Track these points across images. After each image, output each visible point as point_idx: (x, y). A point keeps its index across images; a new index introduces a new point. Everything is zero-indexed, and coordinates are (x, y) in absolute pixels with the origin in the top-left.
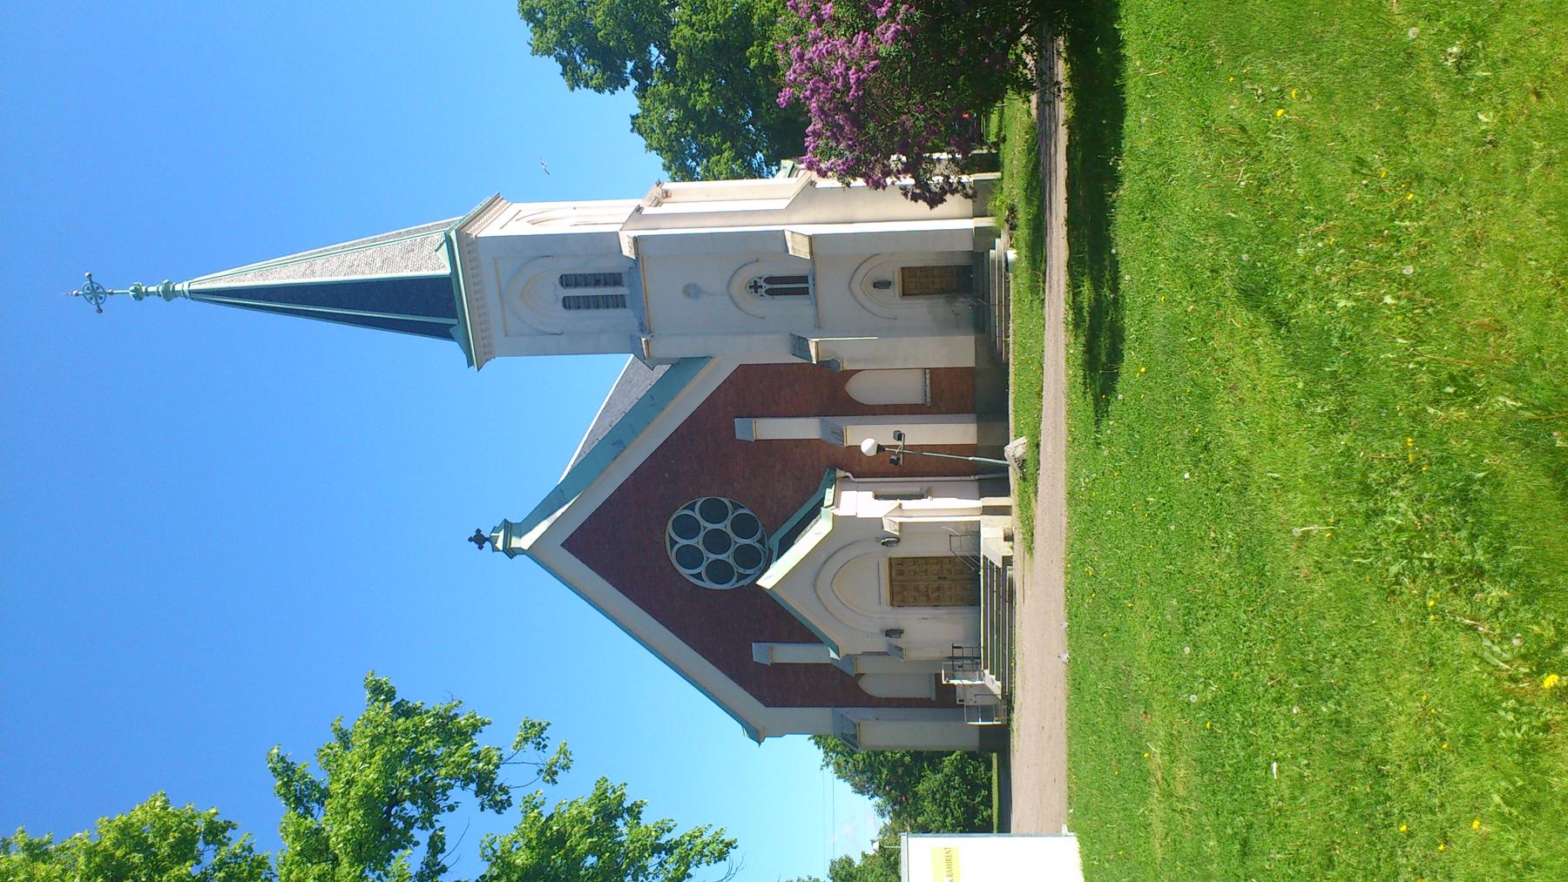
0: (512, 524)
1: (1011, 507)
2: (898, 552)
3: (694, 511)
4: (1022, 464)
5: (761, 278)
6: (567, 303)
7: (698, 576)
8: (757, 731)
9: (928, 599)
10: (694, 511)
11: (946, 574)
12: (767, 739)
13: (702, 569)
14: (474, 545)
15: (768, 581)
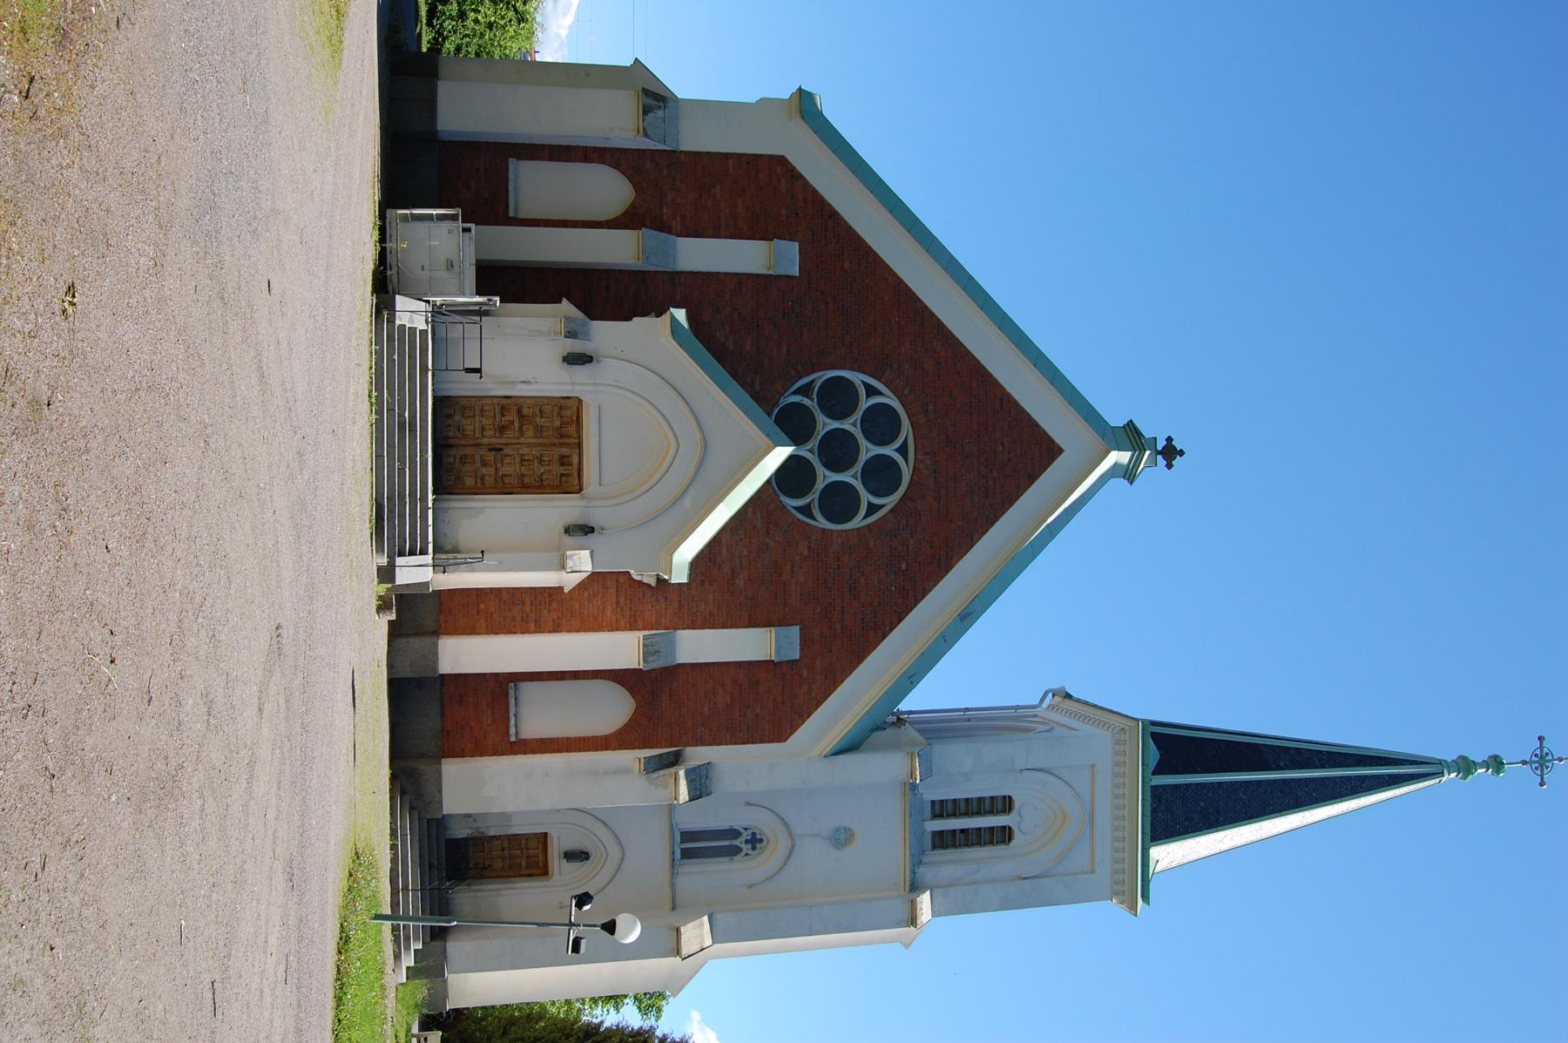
0: (1124, 477)
1: (389, 621)
3: (869, 502)
5: (747, 854)
6: (1004, 804)
7: (871, 391)
8: (803, 118)
9: (519, 411)
11: (491, 456)
12: (787, 96)
13: (865, 403)
14: (1177, 444)
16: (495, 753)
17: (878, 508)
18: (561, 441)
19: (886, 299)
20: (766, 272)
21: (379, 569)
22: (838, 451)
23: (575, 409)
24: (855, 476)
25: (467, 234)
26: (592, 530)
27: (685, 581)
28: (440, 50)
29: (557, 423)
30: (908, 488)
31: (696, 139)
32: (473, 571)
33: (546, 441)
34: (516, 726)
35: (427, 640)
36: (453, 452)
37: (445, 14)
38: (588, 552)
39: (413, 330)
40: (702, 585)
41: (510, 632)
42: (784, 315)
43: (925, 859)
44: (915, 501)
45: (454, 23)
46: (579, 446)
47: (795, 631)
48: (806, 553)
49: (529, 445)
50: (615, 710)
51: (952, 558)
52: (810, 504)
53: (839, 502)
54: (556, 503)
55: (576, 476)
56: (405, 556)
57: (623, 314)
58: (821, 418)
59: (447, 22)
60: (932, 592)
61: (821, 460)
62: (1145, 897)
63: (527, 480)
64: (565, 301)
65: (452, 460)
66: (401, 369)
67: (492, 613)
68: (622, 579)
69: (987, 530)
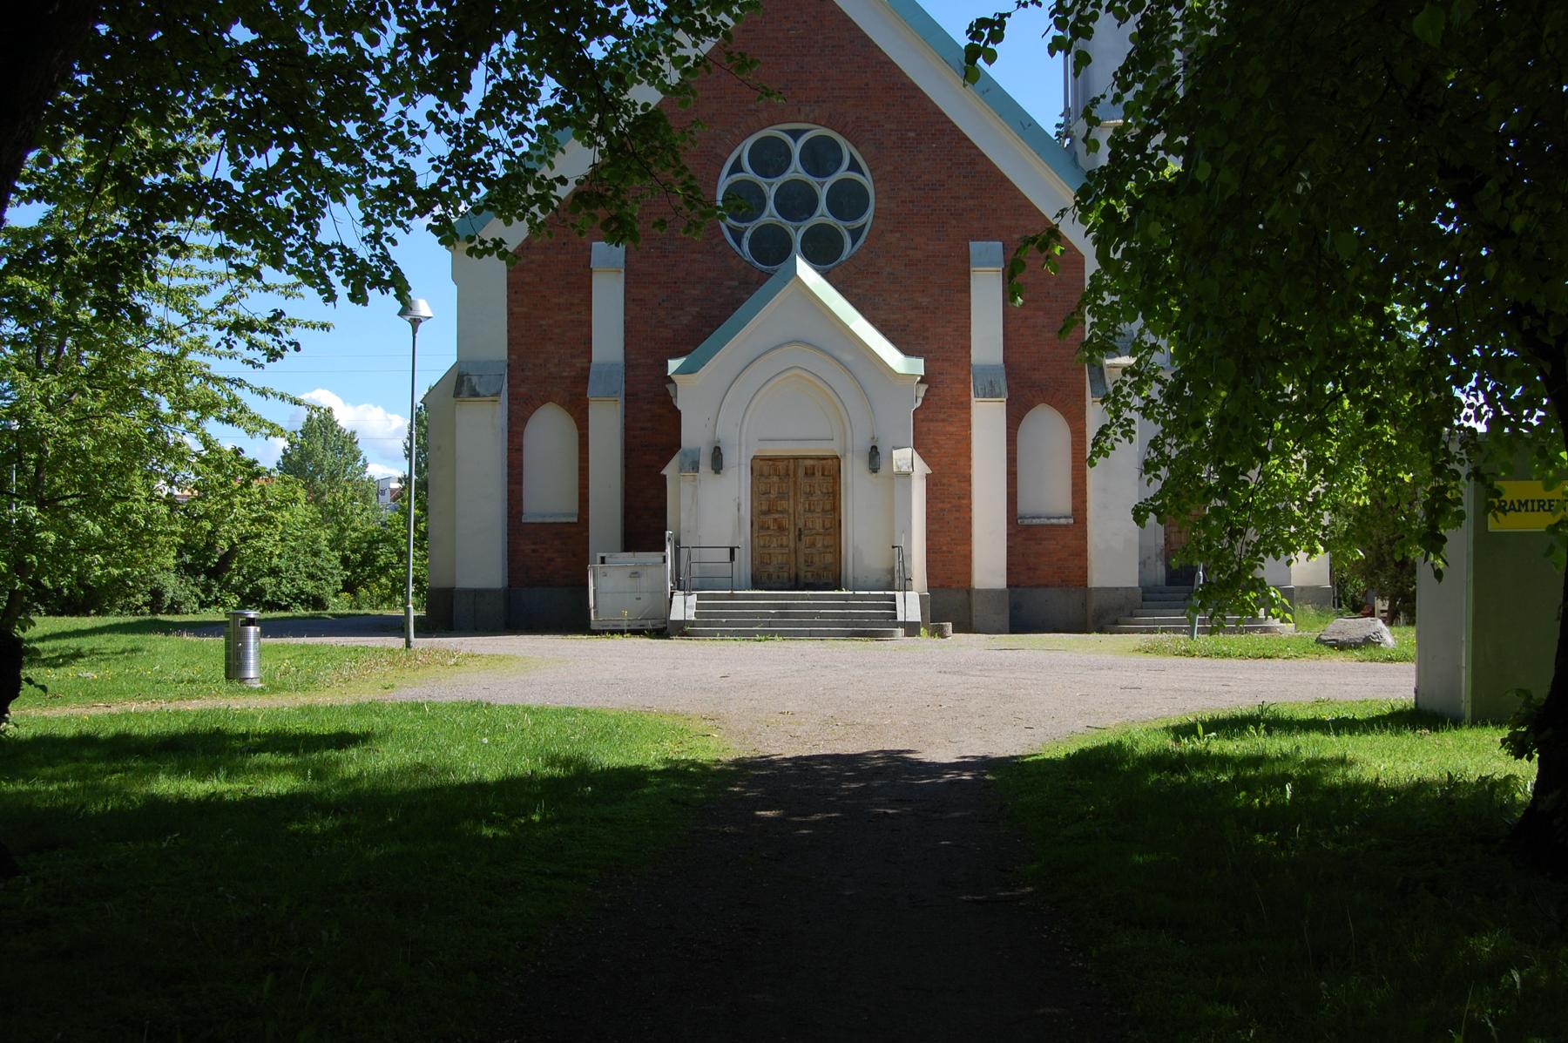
2: (854, 476)
4: (1368, 642)
7: (736, 167)
10: (848, 169)
11: (806, 540)
13: (749, 174)
15: (806, 272)
16: (1085, 538)
17: (853, 161)
18: (792, 476)
20: (623, 275)
21: (907, 635)
22: (796, 202)
23: (761, 463)
24: (822, 184)
25: (606, 560)
26: (874, 448)
27: (923, 360)
28: (314, 597)
29: (775, 479)
31: (496, 345)
32: (910, 556)
33: (792, 488)
34: (1059, 518)
35: (974, 597)
36: (802, 574)
37: (275, 593)
38: (894, 452)
39: (698, 606)
40: (927, 338)
41: (970, 523)
42: (664, 257)
44: (847, 123)
45: (284, 580)
46: (796, 458)
47: (975, 246)
48: (898, 235)
49: (796, 504)
50: (1047, 426)
51: (904, 84)
52: (849, 231)
53: (847, 200)
54: (849, 480)
55: (824, 462)
56: (895, 605)
57: (673, 417)
58: (764, 219)
59: (284, 589)
60: (938, 104)
61: (806, 219)
63: (828, 507)
64: (664, 472)
65: (809, 574)
66: (733, 616)
67: (952, 540)
68: (920, 416)
69: (876, 46)
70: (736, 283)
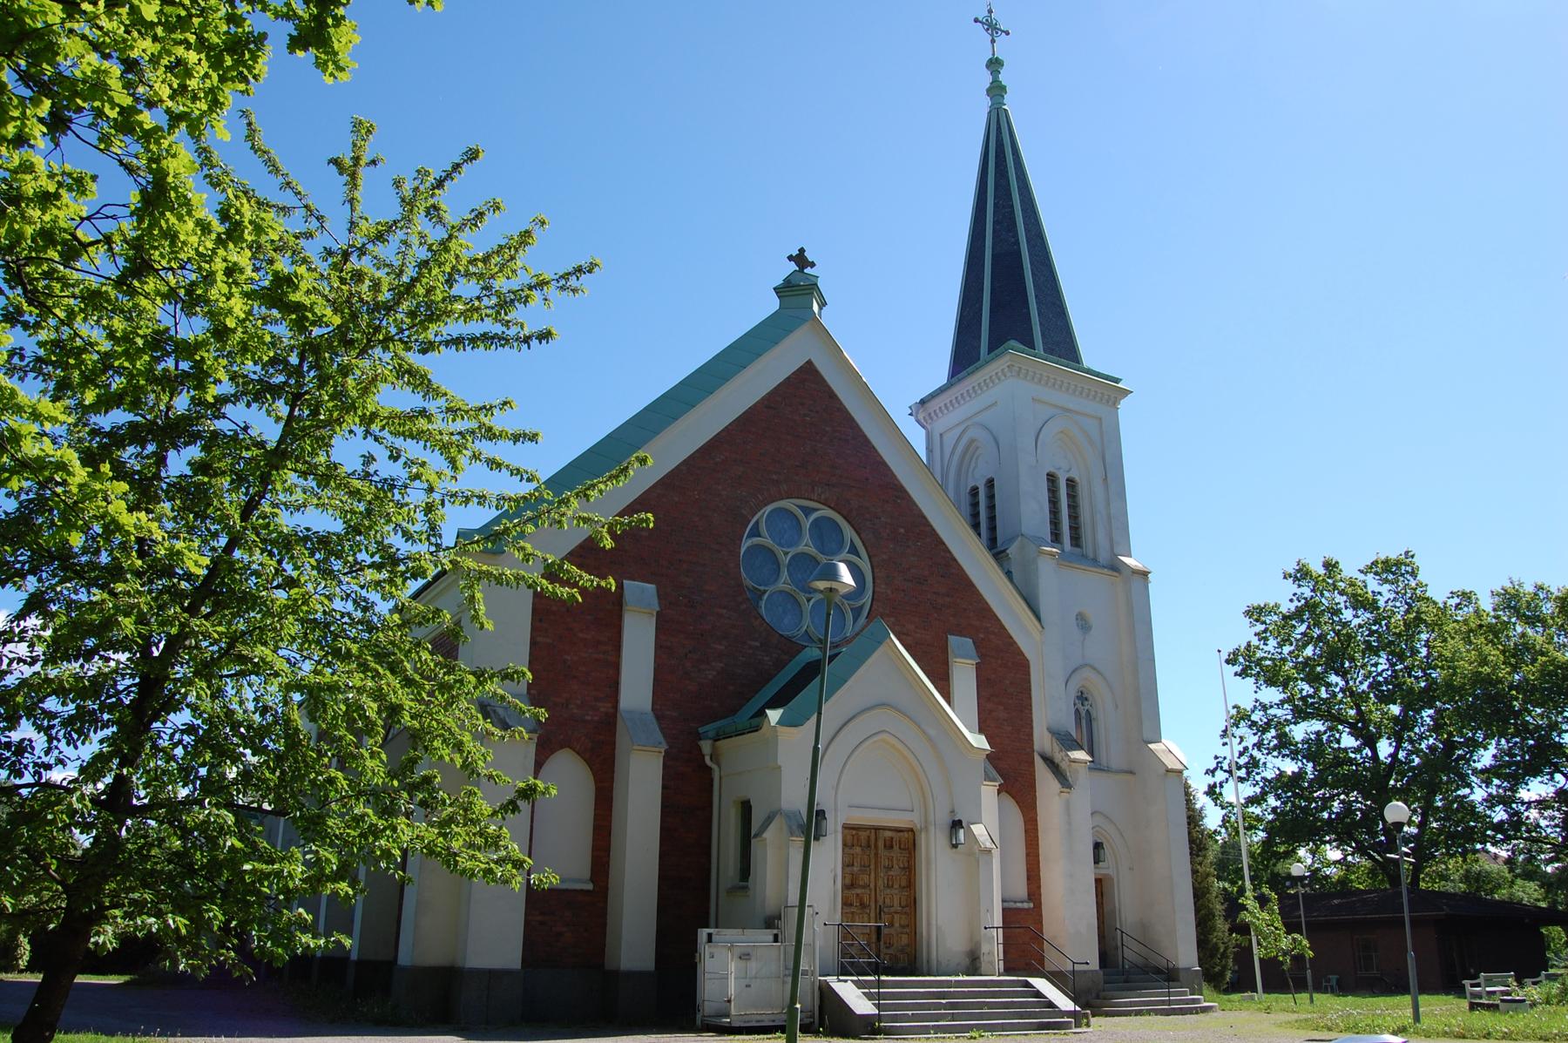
17: (752, 534)
19: (676, 499)
30: (839, 513)
33: (873, 862)
43: (1091, 555)
46: (877, 829)
47: (953, 640)
55: (902, 834)
62: (1117, 381)
63: (904, 883)
70: (758, 644)
